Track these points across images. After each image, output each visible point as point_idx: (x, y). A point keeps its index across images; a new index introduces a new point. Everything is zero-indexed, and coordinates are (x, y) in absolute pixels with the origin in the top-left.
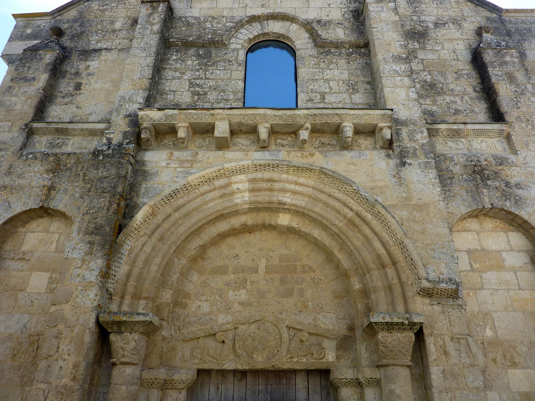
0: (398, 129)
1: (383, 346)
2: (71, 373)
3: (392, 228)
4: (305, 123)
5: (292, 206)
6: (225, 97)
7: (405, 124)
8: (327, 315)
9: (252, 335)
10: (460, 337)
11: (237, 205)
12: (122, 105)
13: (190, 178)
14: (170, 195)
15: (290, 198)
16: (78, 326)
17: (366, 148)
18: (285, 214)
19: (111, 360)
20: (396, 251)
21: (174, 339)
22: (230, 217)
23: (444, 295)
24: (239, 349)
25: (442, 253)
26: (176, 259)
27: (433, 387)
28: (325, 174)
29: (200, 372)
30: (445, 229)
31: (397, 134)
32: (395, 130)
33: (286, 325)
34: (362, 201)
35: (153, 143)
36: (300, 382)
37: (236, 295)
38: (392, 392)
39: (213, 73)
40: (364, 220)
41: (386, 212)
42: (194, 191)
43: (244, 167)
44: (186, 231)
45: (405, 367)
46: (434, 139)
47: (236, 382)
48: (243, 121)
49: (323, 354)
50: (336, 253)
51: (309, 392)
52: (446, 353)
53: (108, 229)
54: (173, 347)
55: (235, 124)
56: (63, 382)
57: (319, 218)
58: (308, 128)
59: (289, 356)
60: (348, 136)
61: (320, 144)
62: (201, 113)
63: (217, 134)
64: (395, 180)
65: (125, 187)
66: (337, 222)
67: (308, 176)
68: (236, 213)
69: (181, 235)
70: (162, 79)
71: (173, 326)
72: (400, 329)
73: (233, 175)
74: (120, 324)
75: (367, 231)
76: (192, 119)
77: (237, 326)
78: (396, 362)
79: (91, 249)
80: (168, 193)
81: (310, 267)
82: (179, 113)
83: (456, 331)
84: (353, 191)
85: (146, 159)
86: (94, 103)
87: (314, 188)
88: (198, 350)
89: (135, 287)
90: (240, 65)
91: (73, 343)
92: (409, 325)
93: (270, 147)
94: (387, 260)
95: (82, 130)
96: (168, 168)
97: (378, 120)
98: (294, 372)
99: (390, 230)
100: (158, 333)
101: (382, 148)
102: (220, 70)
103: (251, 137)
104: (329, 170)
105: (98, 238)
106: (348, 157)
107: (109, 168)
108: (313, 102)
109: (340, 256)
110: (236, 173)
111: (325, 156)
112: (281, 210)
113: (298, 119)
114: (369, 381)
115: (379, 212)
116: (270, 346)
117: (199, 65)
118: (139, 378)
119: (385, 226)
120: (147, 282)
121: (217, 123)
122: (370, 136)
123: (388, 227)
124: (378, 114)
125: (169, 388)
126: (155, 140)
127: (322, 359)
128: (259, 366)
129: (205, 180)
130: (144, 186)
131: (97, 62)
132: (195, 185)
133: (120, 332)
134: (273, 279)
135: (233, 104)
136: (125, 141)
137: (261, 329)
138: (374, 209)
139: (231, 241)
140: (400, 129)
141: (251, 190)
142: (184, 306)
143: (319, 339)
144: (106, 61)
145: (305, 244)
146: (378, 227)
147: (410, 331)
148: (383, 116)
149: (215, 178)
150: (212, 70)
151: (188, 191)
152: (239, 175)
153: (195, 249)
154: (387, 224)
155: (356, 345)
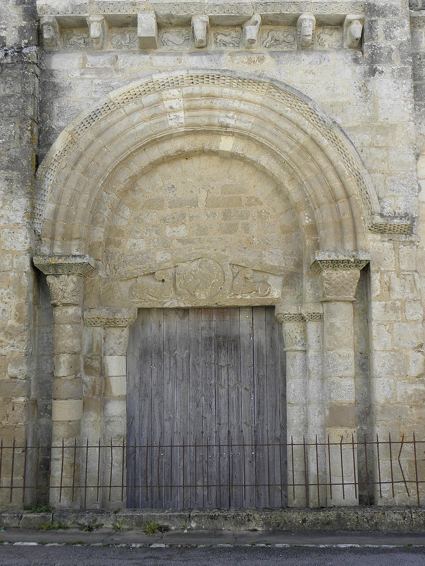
0: (372, 21)
1: (327, 283)
2: (16, 315)
3: (349, 156)
7: (383, 13)
8: (273, 251)
10: (407, 273)
11: (171, 128)
13: (112, 95)
14: (90, 117)
15: (234, 118)
19: (52, 302)
20: (351, 183)
21: (110, 279)
22: (163, 141)
23: (397, 231)
24: (180, 287)
25: (403, 185)
27: (373, 320)
28: (276, 88)
29: (139, 309)
30: (410, 156)
31: (370, 28)
32: (368, 23)
33: (229, 262)
34: (318, 123)
35: (59, 43)
36: (244, 318)
37: (174, 231)
38: (332, 325)
41: (344, 138)
43: (177, 79)
44: (114, 161)
46: (420, 30)
48: (174, 13)
49: (268, 291)
50: (286, 185)
51: (253, 327)
52: (389, 289)
53: (25, 163)
54: (110, 287)
55: (163, 16)
57: (268, 144)
58: (257, 22)
60: (307, 34)
61: (272, 42)
64: (360, 94)
65: (35, 108)
66: (288, 149)
67: (255, 90)
68: (170, 137)
71: (108, 265)
72: (345, 266)
74: (56, 266)
75: (322, 161)
76: (107, 10)
77: (176, 265)
78: (340, 298)
79: (10, 186)
80: (88, 115)
81: (257, 200)
84: (309, 110)
85: (53, 67)
87: (262, 105)
89: (64, 227)
92: (354, 263)
93: (208, 48)
94: (339, 192)
96: (83, 79)
98: (239, 308)
99: (346, 158)
101: (350, 47)
103: (184, 31)
104: (281, 83)
105: (15, 173)
106: (307, 62)
107: (12, 83)
109: (289, 187)
110: (168, 87)
111: (278, 61)
112: (223, 133)
113: (245, 10)
114: (311, 315)
115: (336, 137)
118: (81, 317)
119: (342, 153)
120: (78, 221)
121: (139, 16)
122: (337, 29)
123: (345, 155)
127: (266, 295)
128: (202, 304)
129: (131, 96)
130: (56, 104)
133: (57, 275)
134: (215, 214)
136: (23, 42)
137: (203, 267)
138: (331, 133)
139: (166, 169)
140: (375, 21)
142: (118, 244)
143: (264, 275)
145: (251, 172)
147: (356, 268)
149: (142, 93)
151: (110, 111)
152: (171, 89)
154: (344, 151)
155: (302, 282)
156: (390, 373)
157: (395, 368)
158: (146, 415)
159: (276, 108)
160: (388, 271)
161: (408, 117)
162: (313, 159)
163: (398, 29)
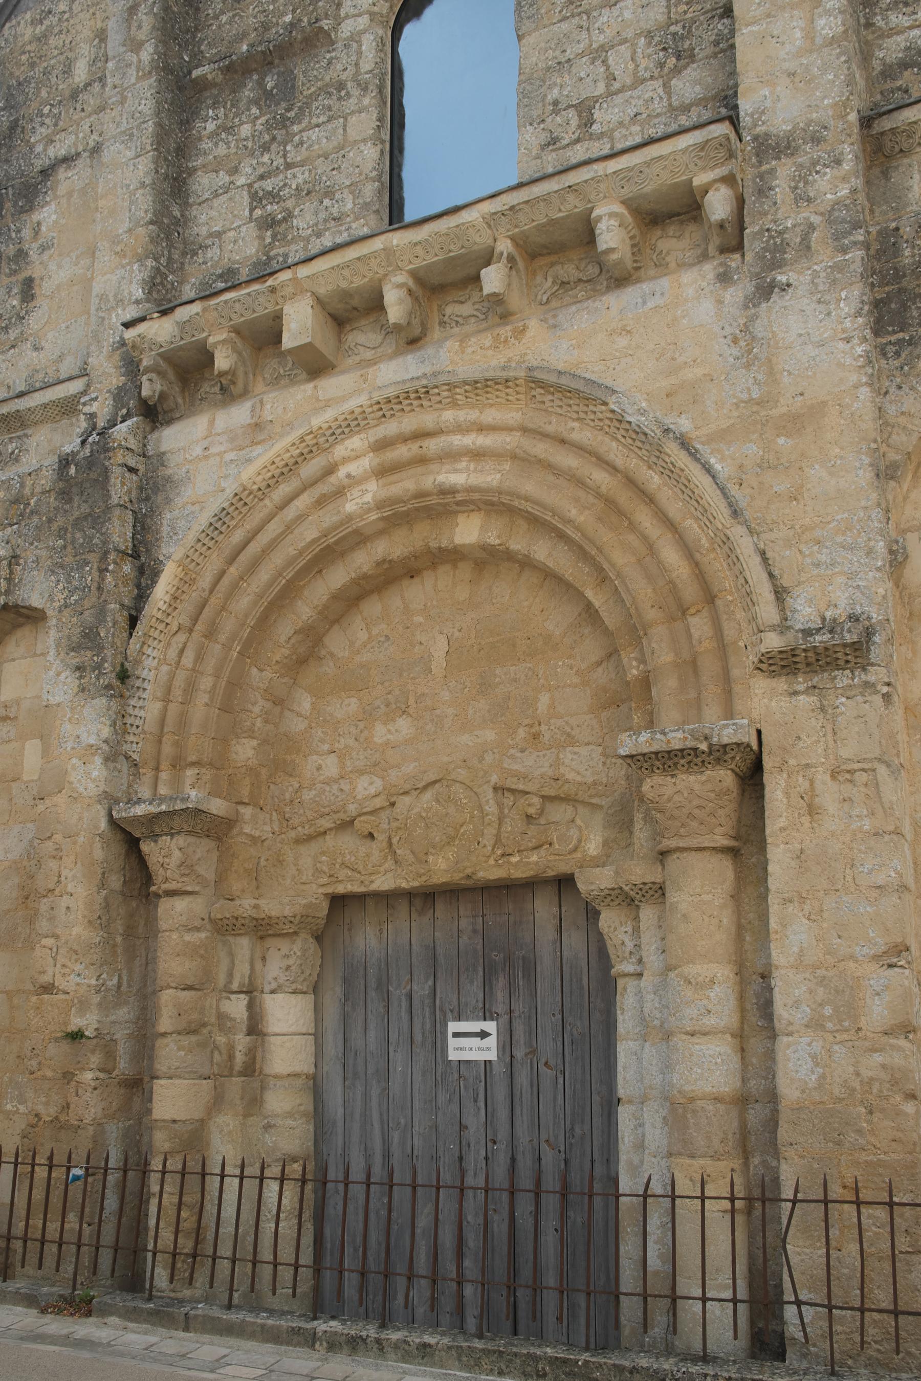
0: (761, 176)
2: (84, 917)
4: (495, 240)
5: (472, 491)
6: (335, 211)
9: (424, 814)
10: (856, 766)
11: (350, 518)
12: (103, 318)
16: (83, 833)
17: (681, 265)
18: (472, 514)
25: (843, 547)
26: (254, 671)
30: (861, 472)
33: (492, 783)
34: (634, 440)
39: (301, 143)
40: (649, 499)
42: (261, 504)
43: (354, 416)
45: (707, 854)
47: (414, 916)
52: (813, 810)
56: (74, 933)
59: (499, 852)
62: (249, 294)
63: (288, 342)
64: (735, 351)
67: (503, 401)
69: (246, 616)
70: (191, 206)
73: (336, 442)
76: (234, 316)
77: (392, 800)
80: (207, 523)
82: (205, 310)
83: (845, 753)
86: (63, 326)
87: (525, 430)
88: (324, 858)
90: (365, 89)
91: (79, 864)
92: (710, 753)
94: (690, 592)
95: (45, 406)
97: (691, 166)
100: (235, 831)
102: (318, 126)
108: (558, 145)
116: (463, 835)
117: (268, 127)
124: (687, 148)
125: (270, 935)
126: (183, 391)
129: (279, 471)
131: (53, 206)
132: (260, 489)
133: (155, 837)
135: (354, 225)
141: (383, 472)
144: (70, 194)
146: (674, 509)
147: (718, 767)
148: (702, 149)
149: (300, 460)
150: (301, 131)
153: (288, 642)
156: (816, 1024)
157: (828, 1011)
158: (357, 1116)
159: (550, 429)
160: (808, 766)
161: (854, 378)
162: (633, 527)
163: (825, 174)
